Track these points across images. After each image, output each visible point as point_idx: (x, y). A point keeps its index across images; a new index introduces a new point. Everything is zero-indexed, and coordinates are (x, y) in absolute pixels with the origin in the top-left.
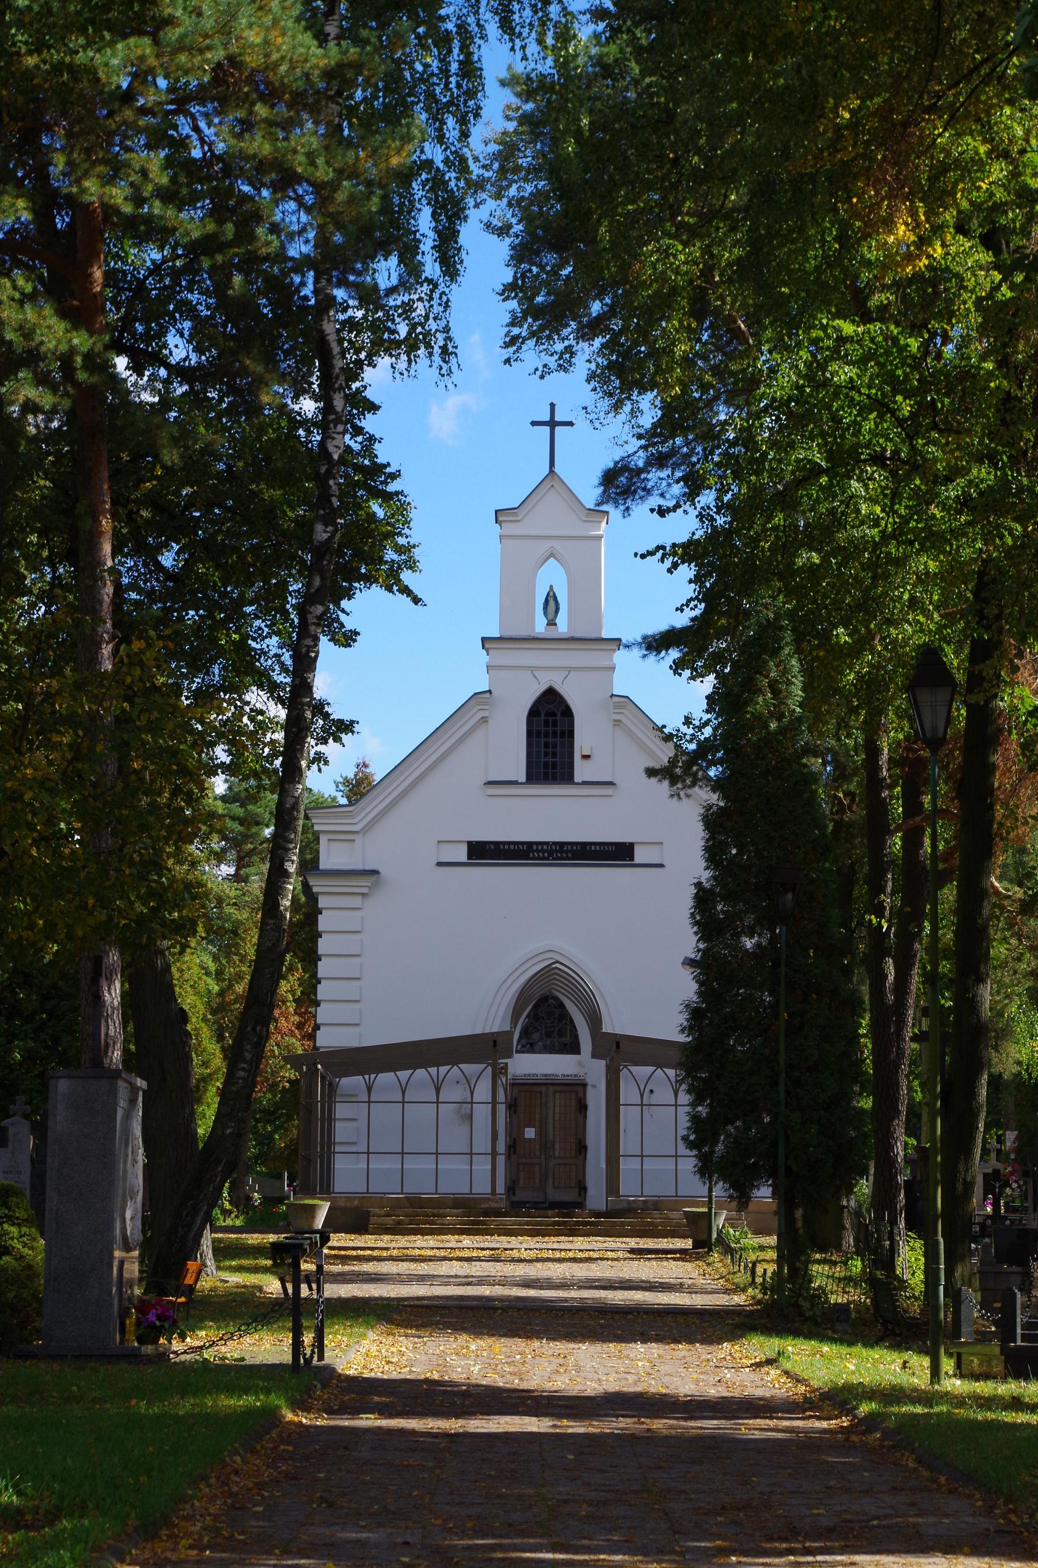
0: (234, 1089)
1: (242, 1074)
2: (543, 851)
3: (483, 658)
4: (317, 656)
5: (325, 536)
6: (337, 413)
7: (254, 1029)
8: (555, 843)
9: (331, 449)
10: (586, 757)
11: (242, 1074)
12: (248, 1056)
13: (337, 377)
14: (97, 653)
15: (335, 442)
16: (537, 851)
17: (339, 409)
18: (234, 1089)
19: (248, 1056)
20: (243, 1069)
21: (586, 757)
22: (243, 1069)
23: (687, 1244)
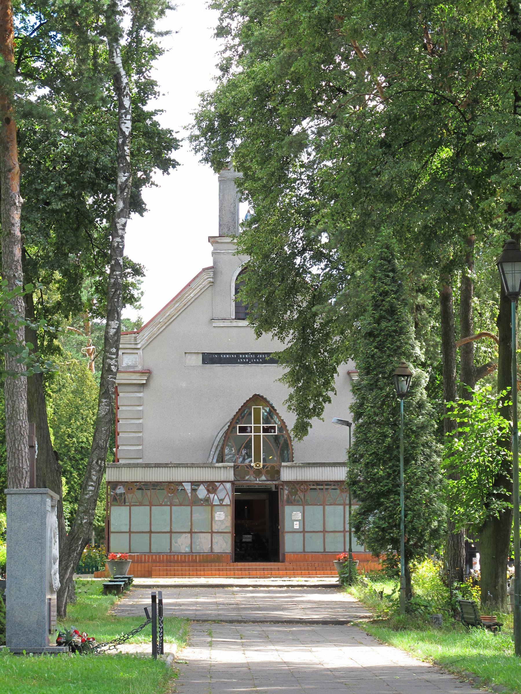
0: (87, 497)
1: (91, 488)
2: (245, 358)
3: (210, 248)
4: (123, 248)
5: (124, 179)
6: (126, 109)
7: (97, 462)
8: (252, 354)
9: (124, 129)
10: (164, 95)
11: (91, 488)
12: (94, 478)
13: (125, 88)
14: (6, 22)
15: (126, 125)
16: (242, 358)
17: (127, 106)
18: (87, 497)
19: (94, 478)
20: (92, 485)
21: (164, 95)
22: (92, 485)
23: (334, 581)
